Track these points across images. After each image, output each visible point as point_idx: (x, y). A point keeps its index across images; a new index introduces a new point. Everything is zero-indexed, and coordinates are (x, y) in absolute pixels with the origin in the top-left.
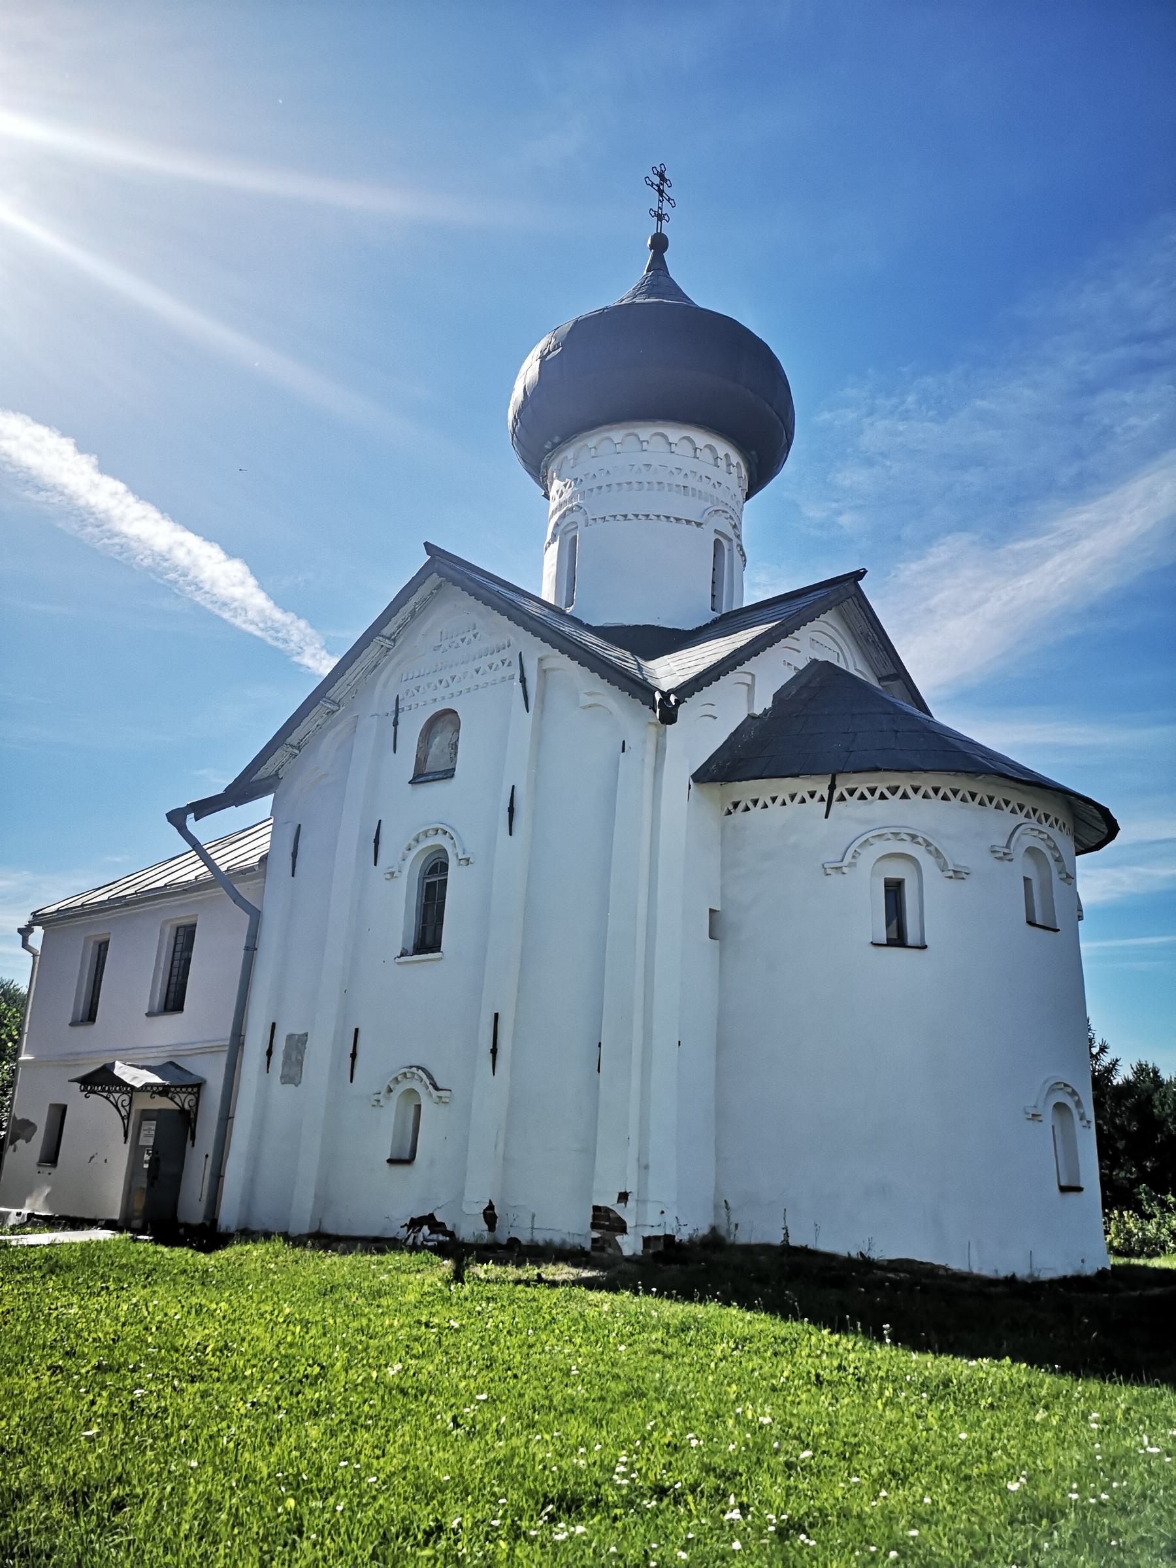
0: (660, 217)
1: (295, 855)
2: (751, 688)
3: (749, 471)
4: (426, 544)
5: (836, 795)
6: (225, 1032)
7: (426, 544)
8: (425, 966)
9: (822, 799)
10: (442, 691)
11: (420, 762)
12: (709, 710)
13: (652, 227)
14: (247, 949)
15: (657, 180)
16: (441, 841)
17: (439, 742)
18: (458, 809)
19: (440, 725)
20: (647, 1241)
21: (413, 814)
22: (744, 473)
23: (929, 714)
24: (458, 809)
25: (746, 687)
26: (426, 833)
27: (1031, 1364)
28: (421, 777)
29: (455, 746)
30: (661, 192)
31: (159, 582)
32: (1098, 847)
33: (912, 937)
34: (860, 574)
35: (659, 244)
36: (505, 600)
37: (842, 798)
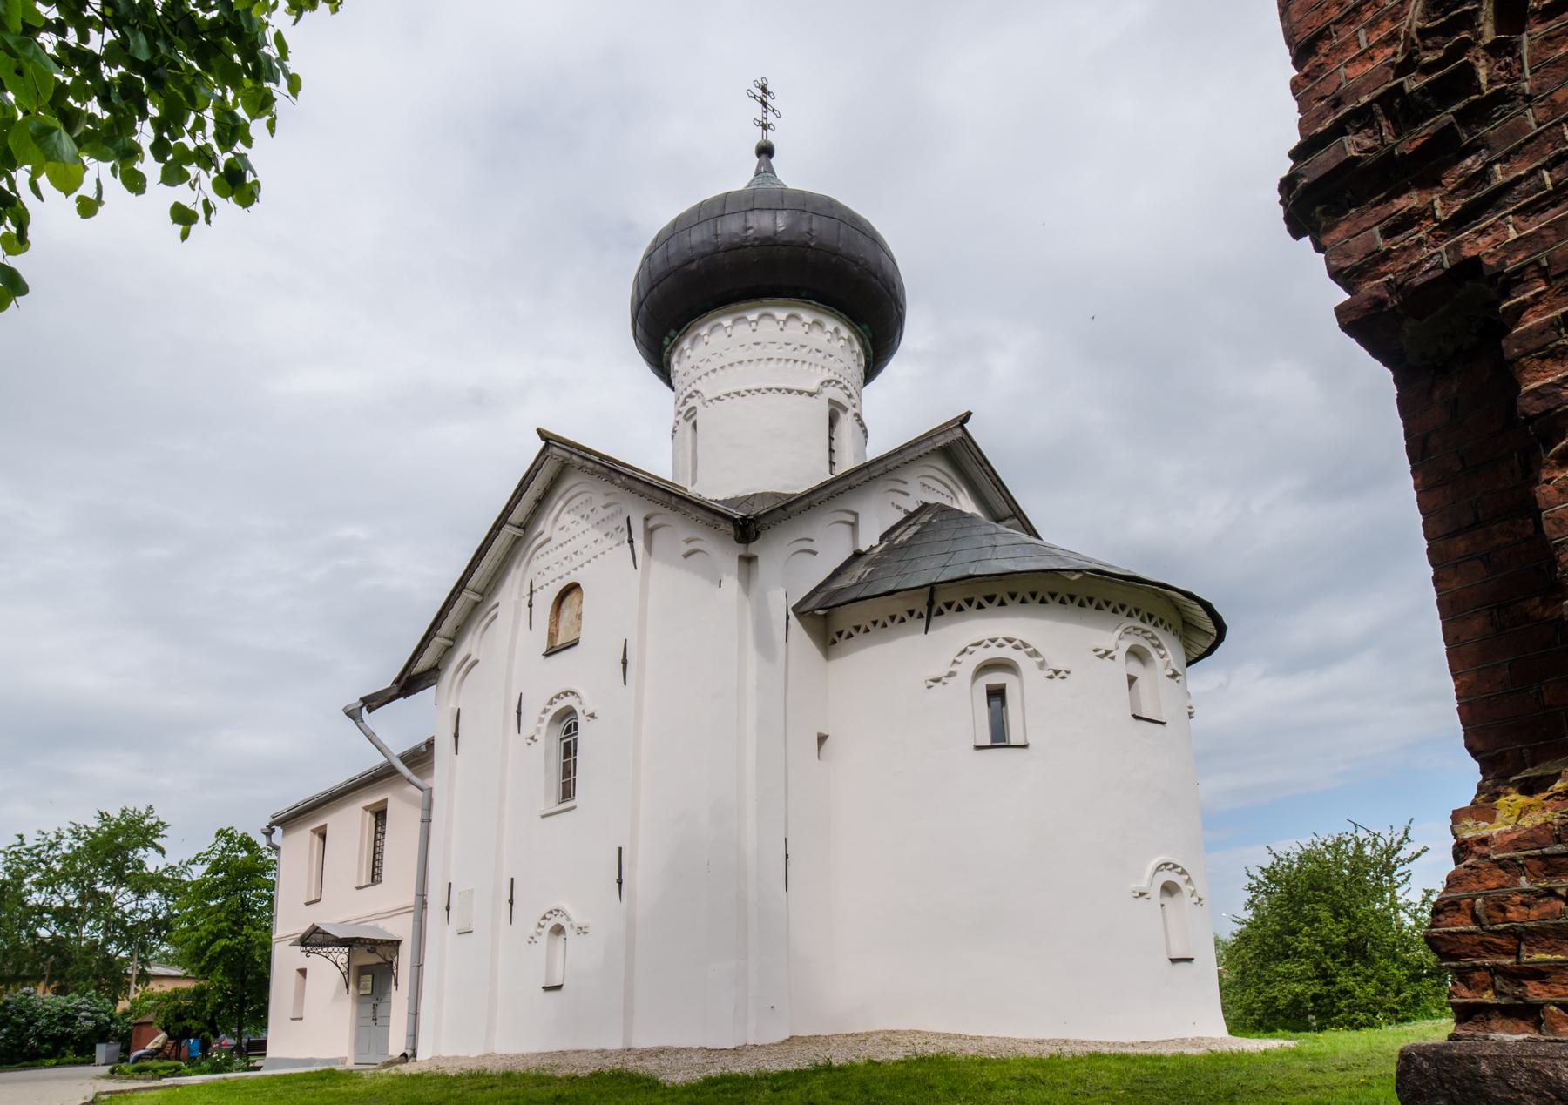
0: (765, 127)
1: (456, 736)
2: (854, 526)
3: (863, 346)
4: (539, 431)
5: (934, 611)
6: (410, 899)
7: (539, 431)
9: (921, 616)
10: (568, 566)
11: (552, 636)
12: (807, 546)
13: (756, 136)
14: (423, 821)
15: (759, 93)
16: (570, 701)
17: (567, 612)
18: (585, 675)
19: (568, 600)
21: (544, 680)
22: (857, 347)
23: (1038, 537)
24: (585, 675)
25: (847, 528)
26: (558, 697)
27: (1357, 205)
28: (551, 652)
29: (579, 616)
30: (764, 104)
31: (1556, 961)
32: (1210, 651)
34: (967, 416)
35: (765, 151)
36: (610, 471)
37: (940, 613)
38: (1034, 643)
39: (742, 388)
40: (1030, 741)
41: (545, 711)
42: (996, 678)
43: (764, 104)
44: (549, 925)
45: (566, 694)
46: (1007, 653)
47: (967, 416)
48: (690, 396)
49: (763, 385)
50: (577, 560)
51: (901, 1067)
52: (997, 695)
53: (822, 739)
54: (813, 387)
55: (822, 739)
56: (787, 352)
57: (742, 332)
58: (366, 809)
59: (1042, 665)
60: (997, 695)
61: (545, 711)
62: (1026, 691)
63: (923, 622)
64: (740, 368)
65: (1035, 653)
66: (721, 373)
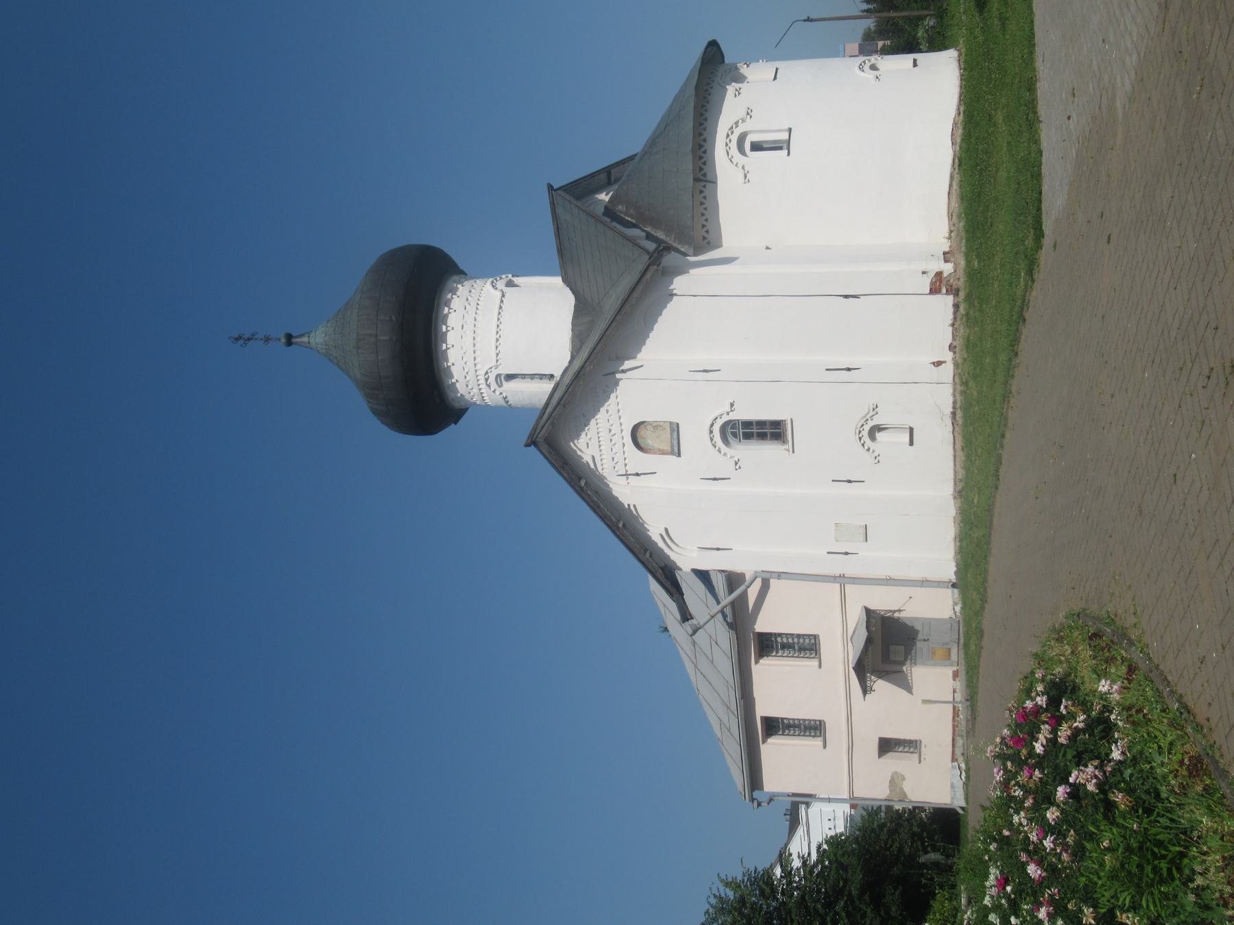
8: (800, 433)
11: (663, 453)
20: (946, 261)
30: (249, 339)
33: (785, 136)
34: (550, 187)
37: (704, 175)
38: (731, 122)
39: (494, 337)
40: (786, 127)
41: (719, 451)
42: (747, 146)
43: (249, 339)
44: (866, 438)
45: (711, 432)
46: (734, 138)
47: (550, 187)
48: (487, 380)
49: (495, 322)
50: (615, 429)
51: (957, 429)
52: (756, 147)
53: (767, 248)
54: (499, 294)
55: (767, 248)
56: (471, 309)
57: (451, 338)
58: (757, 662)
59: (743, 121)
60: (756, 147)
61: (719, 451)
62: (762, 127)
63: (708, 185)
64: (478, 339)
65: (737, 123)
66: (478, 353)
